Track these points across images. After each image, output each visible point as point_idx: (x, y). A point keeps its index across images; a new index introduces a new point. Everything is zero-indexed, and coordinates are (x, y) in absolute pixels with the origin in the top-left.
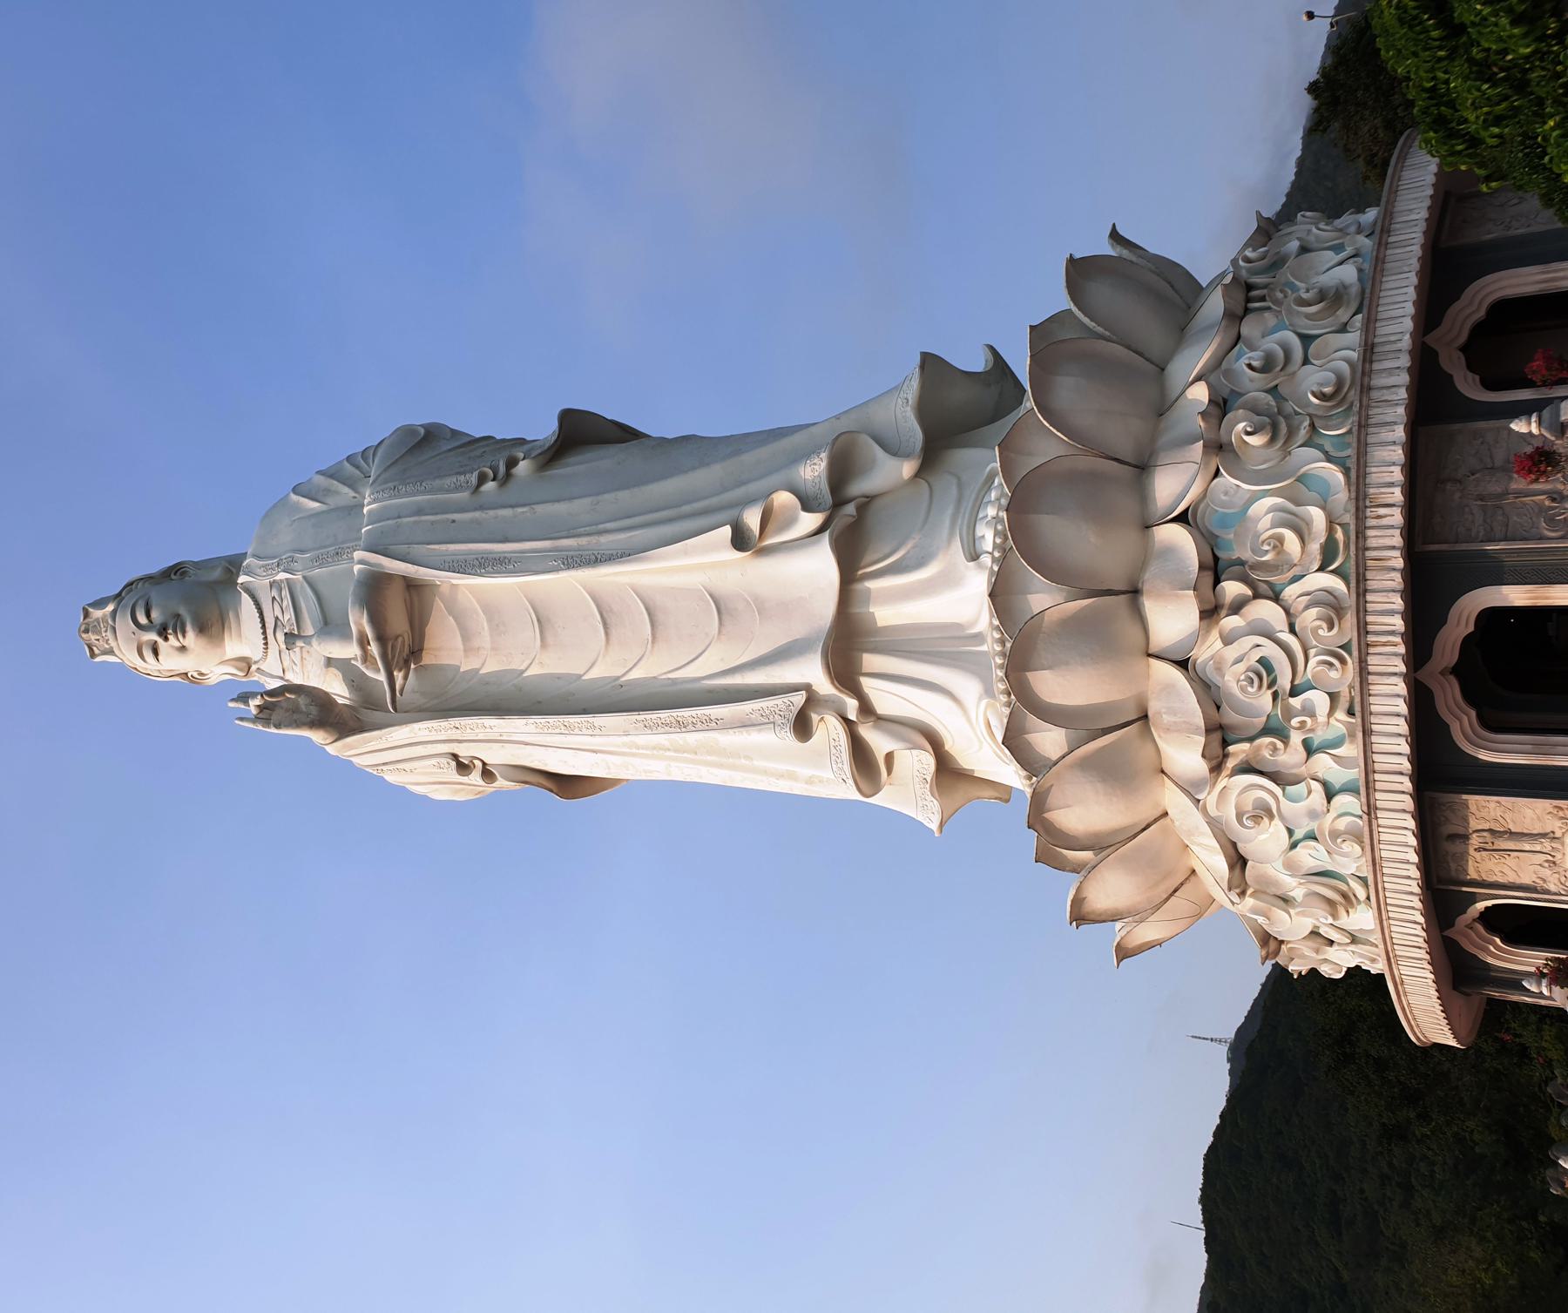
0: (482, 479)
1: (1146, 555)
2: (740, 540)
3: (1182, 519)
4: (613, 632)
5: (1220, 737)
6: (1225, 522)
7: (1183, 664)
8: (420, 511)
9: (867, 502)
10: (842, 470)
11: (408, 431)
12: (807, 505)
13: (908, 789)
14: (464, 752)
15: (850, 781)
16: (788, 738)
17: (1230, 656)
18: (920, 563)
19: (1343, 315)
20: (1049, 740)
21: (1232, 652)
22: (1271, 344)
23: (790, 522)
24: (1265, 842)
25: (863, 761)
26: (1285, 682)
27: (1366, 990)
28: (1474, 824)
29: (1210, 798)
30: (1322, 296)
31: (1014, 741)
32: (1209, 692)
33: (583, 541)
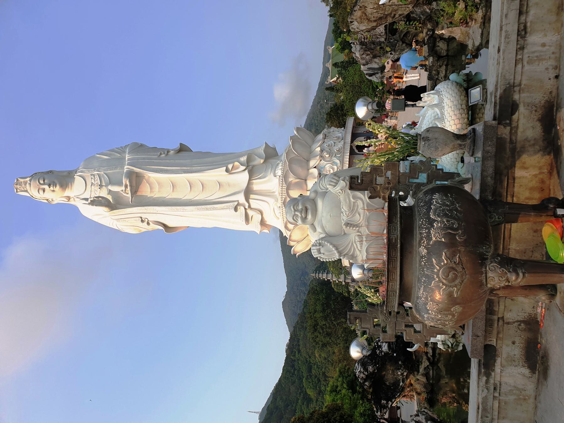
0: (161, 154)
1: (308, 174)
2: (227, 170)
3: (315, 167)
4: (192, 188)
6: (322, 168)
8: (144, 159)
10: (248, 161)
11: (136, 144)
12: (242, 165)
13: (254, 227)
14: (144, 216)
16: (233, 211)
18: (264, 178)
19: (340, 140)
22: (329, 143)
23: (238, 168)
25: (247, 219)
30: (336, 137)
33: (188, 168)
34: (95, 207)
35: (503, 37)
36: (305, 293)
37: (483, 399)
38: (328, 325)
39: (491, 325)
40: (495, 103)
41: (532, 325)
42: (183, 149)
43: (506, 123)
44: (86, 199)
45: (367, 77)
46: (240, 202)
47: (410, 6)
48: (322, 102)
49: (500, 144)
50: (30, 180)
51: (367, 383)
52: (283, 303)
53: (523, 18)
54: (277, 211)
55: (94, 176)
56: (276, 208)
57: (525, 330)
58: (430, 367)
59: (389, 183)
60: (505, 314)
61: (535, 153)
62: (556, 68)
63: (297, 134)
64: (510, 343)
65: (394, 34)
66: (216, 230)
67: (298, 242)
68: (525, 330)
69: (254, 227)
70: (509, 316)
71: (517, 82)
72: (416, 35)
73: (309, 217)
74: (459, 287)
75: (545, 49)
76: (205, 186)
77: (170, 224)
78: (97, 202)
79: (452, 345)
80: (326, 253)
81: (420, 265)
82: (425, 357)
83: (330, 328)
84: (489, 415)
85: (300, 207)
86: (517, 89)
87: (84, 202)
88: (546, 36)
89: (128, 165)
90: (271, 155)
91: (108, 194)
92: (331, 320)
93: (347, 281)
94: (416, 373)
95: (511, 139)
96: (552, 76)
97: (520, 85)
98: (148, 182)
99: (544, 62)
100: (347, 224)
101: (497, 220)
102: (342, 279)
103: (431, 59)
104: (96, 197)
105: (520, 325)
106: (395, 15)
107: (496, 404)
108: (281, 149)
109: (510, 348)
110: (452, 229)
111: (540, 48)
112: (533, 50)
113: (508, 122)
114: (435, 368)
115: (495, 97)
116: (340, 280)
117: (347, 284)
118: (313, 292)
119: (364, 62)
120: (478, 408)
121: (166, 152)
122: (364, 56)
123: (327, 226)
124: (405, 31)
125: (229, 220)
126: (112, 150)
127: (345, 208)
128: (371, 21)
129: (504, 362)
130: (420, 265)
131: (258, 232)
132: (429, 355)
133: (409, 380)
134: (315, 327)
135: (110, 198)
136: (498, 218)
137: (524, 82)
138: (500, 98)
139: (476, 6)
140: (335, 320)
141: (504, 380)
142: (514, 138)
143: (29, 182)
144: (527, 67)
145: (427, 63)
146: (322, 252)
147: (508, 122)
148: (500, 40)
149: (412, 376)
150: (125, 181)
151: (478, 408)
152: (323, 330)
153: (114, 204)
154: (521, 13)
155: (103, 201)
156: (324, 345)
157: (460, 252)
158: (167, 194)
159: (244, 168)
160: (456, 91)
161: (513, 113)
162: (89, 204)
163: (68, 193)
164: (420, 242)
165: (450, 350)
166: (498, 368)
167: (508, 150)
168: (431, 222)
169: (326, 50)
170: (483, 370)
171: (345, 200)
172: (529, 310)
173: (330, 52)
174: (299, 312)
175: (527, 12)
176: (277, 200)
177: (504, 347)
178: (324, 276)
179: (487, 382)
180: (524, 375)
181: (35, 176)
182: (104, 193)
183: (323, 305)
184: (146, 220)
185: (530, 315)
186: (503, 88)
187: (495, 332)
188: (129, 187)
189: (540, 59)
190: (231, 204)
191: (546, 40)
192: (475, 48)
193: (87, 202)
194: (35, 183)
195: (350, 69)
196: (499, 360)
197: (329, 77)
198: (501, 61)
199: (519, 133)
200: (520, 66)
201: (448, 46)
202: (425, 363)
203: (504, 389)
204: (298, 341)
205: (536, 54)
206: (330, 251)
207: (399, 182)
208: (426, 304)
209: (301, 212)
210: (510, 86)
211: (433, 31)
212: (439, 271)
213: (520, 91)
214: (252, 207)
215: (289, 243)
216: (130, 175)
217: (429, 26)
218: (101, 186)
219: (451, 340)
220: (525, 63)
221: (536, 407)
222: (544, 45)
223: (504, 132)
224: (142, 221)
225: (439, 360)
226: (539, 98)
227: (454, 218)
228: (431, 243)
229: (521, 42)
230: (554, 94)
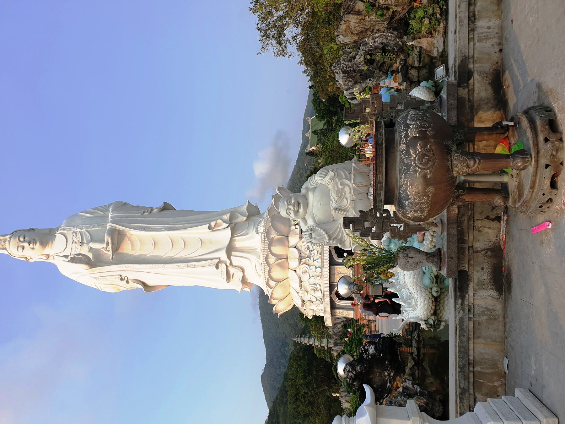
0: (144, 212)
1: (290, 231)
2: (210, 228)
4: (174, 246)
5: (301, 258)
7: (295, 247)
8: (127, 216)
9: (236, 224)
10: (231, 218)
12: (225, 222)
13: (236, 285)
14: (123, 274)
15: (225, 279)
16: (214, 268)
17: (303, 245)
18: (247, 234)
20: (272, 259)
21: (303, 244)
23: (220, 225)
24: (305, 278)
25: (228, 276)
26: (311, 249)
27: (322, 318)
28: (336, 272)
29: (297, 270)
31: (266, 259)
32: (299, 251)
34: (74, 264)
35: (458, 22)
36: (285, 366)
37: (459, 319)
38: (309, 393)
39: (463, 253)
40: (455, 71)
41: (497, 252)
42: (166, 207)
43: (465, 86)
44: (66, 257)
45: (350, 101)
46: (222, 259)
47: (385, 23)
48: (301, 172)
49: (461, 102)
50: (10, 238)
51: (355, 383)
52: (262, 376)
53: (472, 8)
54: (259, 268)
55: (76, 234)
56: (258, 265)
57: (491, 257)
58: (416, 368)
59: (375, 111)
60: (474, 243)
61: (489, 109)
62: (500, 44)
63: (279, 193)
64: (480, 269)
65: (372, 64)
66: (196, 289)
67: (280, 300)
68: (491, 257)
69: (236, 285)
70: (478, 245)
71: (471, 55)
72: (391, 66)
73: (301, 210)
74: (431, 169)
75: (490, 30)
76: (186, 243)
77: (149, 283)
78: (77, 259)
79: (434, 322)
80: (317, 238)
81: (401, 158)
82: (410, 358)
83: (312, 396)
84: (465, 334)
85: (293, 201)
86: (471, 60)
87: (64, 259)
88: (490, 21)
89: (111, 222)
90: (253, 213)
91: (89, 251)
92: (313, 388)
93: (330, 345)
94: (402, 375)
95: (469, 99)
96: (497, 50)
97: (473, 57)
98: (129, 240)
99: (490, 40)
100: (336, 209)
101: (459, 138)
102: (324, 344)
103: (405, 84)
104: (76, 254)
105: (486, 253)
106: (373, 30)
107: (471, 325)
108: (264, 209)
109: (480, 274)
110: (424, 127)
111: (486, 30)
112: (481, 31)
113: (466, 85)
114: (420, 368)
115: (455, 67)
116: (322, 345)
117: (330, 348)
118: (295, 358)
119: (346, 87)
120: (456, 330)
121: (149, 211)
122: (346, 83)
123: (318, 214)
124: (381, 61)
125: (210, 278)
126: (96, 209)
127: (334, 196)
128: (354, 34)
129: (476, 287)
130: (401, 158)
131: (239, 291)
132: (414, 356)
133: (395, 383)
134: (296, 396)
135: (90, 255)
136: (461, 137)
137: (476, 56)
138: (458, 67)
139: (438, 21)
140: (317, 388)
141: (476, 302)
142: (471, 98)
143: (8, 239)
144: (477, 45)
145: (401, 87)
146: (313, 236)
147: (466, 85)
148: (456, 25)
149: (398, 378)
150: (107, 238)
151: (456, 330)
152: (304, 399)
153: (94, 262)
154: (470, 4)
155: (83, 258)
156: (306, 416)
157: (430, 142)
158: (149, 251)
159: (226, 225)
160: (426, 92)
161: (469, 79)
162: (69, 261)
163: (48, 250)
164: (400, 141)
165: (432, 330)
166: (471, 293)
167: (467, 107)
168: (408, 126)
169: (305, 122)
170: (458, 294)
171: (334, 188)
172: (493, 239)
173: (310, 122)
174: (278, 386)
175: (475, 4)
176: (259, 257)
177: (475, 273)
178: (306, 341)
179: (462, 304)
180: (493, 297)
181: (14, 234)
182: (84, 250)
183: (305, 371)
184: (126, 278)
185: (494, 243)
186: (460, 59)
187: (466, 259)
188: (110, 245)
189: (487, 38)
190: (213, 261)
191: (491, 24)
192: (440, 54)
193: (67, 260)
194: (14, 241)
195: (329, 135)
196: (471, 285)
197: (309, 146)
198: (458, 39)
199: (475, 95)
200: (472, 43)
201: (418, 73)
202: (411, 363)
203: (477, 310)
204: (278, 418)
205: (484, 35)
206: (320, 235)
207: (383, 110)
208: (406, 190)
209: (294, 206)
210: (466, 58)
211: (405, 60)
212: (415, 158)
213: (473, 62)
214: (233, 264)
215: (270, 301)
216: (113, 232)
217: (402, 57)
218: (82, 243)
219: (433, 317)
220: (476, 41)
221: (505, 324)
222: (489, 28)
223: (463, 92)
224: (122, 279)
225: (423, 360)
226: (488, 67)
227: (425, 121)
228: (409, 139)
229: (472, 25)
230: (499, 64)
